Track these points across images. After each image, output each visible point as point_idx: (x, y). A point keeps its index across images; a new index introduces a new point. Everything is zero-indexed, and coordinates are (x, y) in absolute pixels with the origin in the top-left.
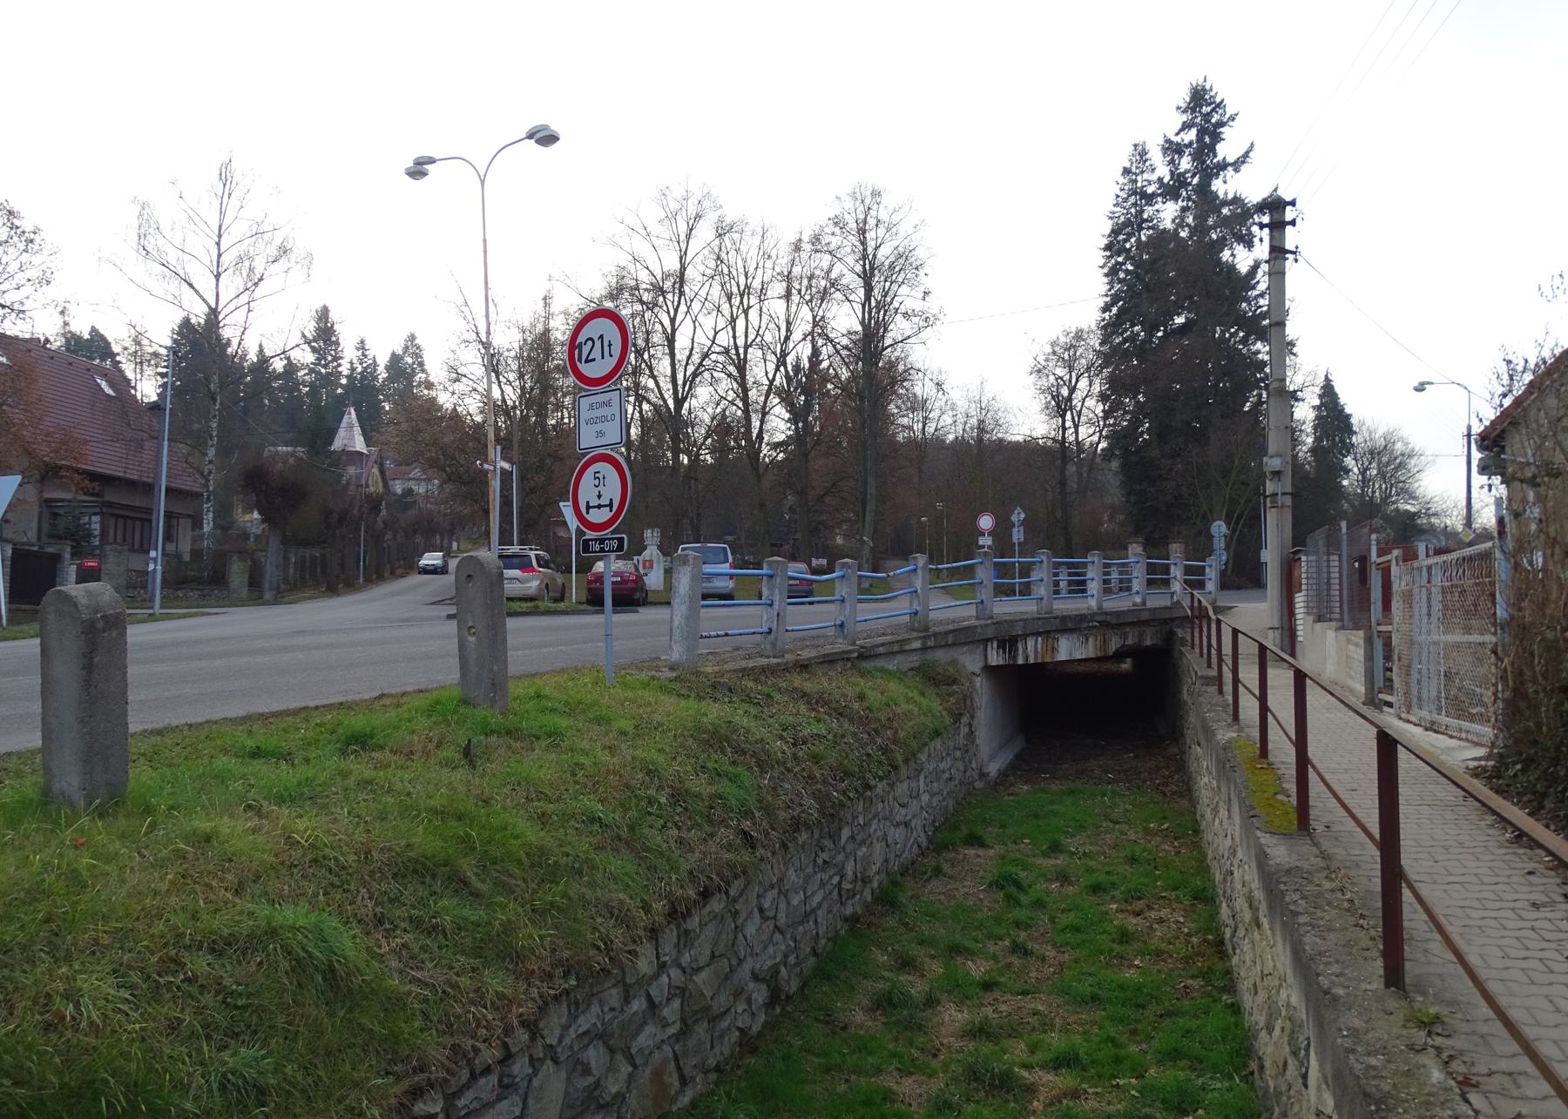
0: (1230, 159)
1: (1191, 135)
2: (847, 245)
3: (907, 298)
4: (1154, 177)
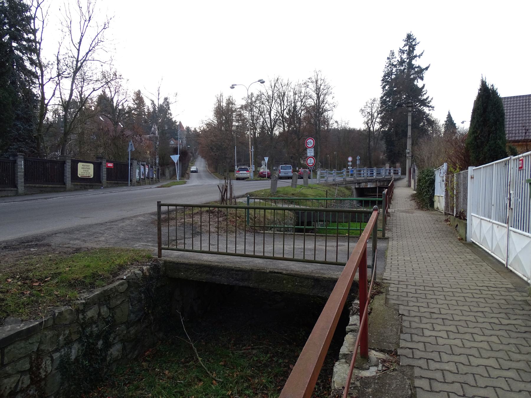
1: (407, 48)
2: (312, 86)
3: (328, 98)
4: (396, 60)
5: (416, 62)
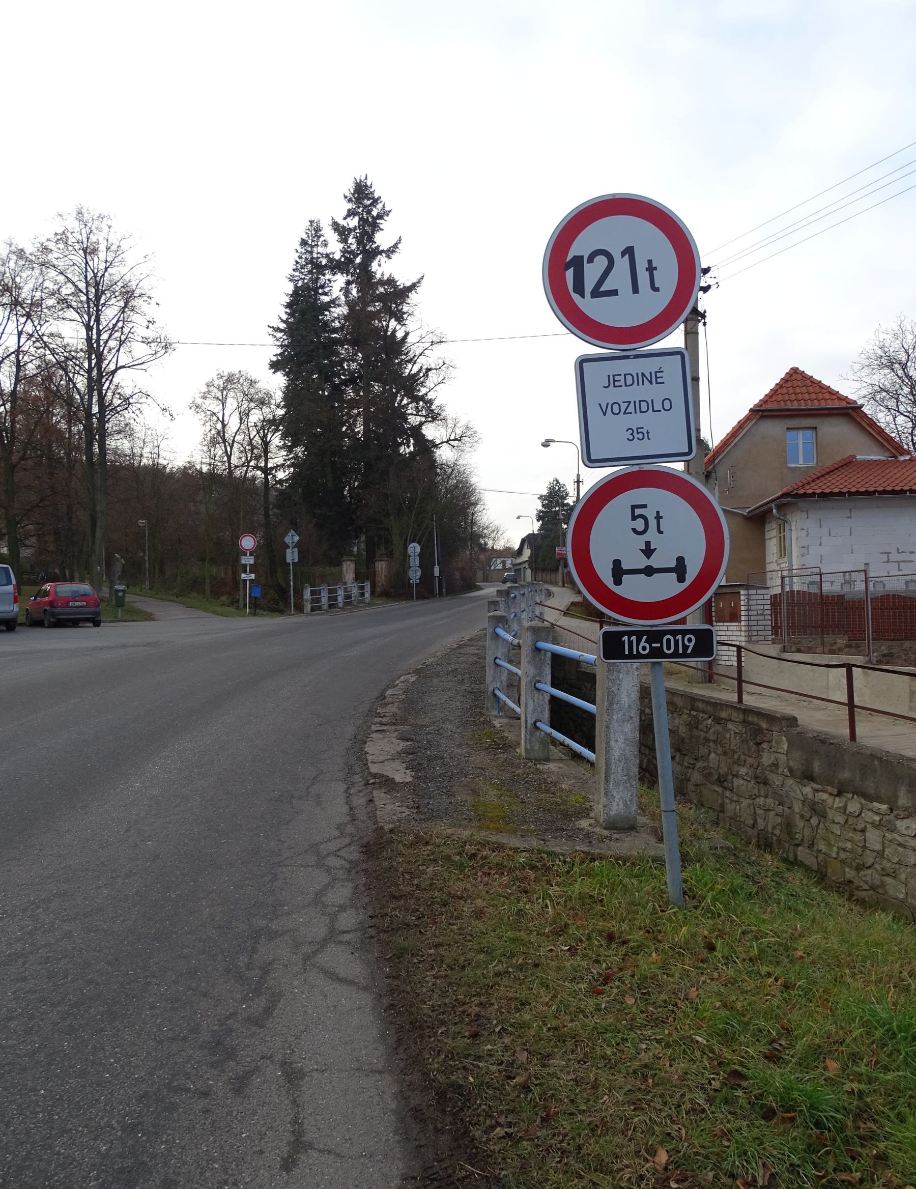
0: (384, 247)
1: (353, 222)
5: (381, 268)
